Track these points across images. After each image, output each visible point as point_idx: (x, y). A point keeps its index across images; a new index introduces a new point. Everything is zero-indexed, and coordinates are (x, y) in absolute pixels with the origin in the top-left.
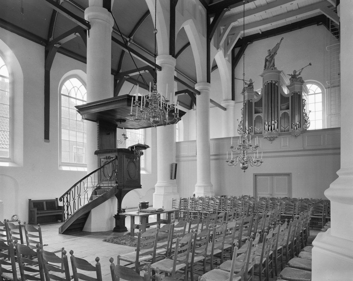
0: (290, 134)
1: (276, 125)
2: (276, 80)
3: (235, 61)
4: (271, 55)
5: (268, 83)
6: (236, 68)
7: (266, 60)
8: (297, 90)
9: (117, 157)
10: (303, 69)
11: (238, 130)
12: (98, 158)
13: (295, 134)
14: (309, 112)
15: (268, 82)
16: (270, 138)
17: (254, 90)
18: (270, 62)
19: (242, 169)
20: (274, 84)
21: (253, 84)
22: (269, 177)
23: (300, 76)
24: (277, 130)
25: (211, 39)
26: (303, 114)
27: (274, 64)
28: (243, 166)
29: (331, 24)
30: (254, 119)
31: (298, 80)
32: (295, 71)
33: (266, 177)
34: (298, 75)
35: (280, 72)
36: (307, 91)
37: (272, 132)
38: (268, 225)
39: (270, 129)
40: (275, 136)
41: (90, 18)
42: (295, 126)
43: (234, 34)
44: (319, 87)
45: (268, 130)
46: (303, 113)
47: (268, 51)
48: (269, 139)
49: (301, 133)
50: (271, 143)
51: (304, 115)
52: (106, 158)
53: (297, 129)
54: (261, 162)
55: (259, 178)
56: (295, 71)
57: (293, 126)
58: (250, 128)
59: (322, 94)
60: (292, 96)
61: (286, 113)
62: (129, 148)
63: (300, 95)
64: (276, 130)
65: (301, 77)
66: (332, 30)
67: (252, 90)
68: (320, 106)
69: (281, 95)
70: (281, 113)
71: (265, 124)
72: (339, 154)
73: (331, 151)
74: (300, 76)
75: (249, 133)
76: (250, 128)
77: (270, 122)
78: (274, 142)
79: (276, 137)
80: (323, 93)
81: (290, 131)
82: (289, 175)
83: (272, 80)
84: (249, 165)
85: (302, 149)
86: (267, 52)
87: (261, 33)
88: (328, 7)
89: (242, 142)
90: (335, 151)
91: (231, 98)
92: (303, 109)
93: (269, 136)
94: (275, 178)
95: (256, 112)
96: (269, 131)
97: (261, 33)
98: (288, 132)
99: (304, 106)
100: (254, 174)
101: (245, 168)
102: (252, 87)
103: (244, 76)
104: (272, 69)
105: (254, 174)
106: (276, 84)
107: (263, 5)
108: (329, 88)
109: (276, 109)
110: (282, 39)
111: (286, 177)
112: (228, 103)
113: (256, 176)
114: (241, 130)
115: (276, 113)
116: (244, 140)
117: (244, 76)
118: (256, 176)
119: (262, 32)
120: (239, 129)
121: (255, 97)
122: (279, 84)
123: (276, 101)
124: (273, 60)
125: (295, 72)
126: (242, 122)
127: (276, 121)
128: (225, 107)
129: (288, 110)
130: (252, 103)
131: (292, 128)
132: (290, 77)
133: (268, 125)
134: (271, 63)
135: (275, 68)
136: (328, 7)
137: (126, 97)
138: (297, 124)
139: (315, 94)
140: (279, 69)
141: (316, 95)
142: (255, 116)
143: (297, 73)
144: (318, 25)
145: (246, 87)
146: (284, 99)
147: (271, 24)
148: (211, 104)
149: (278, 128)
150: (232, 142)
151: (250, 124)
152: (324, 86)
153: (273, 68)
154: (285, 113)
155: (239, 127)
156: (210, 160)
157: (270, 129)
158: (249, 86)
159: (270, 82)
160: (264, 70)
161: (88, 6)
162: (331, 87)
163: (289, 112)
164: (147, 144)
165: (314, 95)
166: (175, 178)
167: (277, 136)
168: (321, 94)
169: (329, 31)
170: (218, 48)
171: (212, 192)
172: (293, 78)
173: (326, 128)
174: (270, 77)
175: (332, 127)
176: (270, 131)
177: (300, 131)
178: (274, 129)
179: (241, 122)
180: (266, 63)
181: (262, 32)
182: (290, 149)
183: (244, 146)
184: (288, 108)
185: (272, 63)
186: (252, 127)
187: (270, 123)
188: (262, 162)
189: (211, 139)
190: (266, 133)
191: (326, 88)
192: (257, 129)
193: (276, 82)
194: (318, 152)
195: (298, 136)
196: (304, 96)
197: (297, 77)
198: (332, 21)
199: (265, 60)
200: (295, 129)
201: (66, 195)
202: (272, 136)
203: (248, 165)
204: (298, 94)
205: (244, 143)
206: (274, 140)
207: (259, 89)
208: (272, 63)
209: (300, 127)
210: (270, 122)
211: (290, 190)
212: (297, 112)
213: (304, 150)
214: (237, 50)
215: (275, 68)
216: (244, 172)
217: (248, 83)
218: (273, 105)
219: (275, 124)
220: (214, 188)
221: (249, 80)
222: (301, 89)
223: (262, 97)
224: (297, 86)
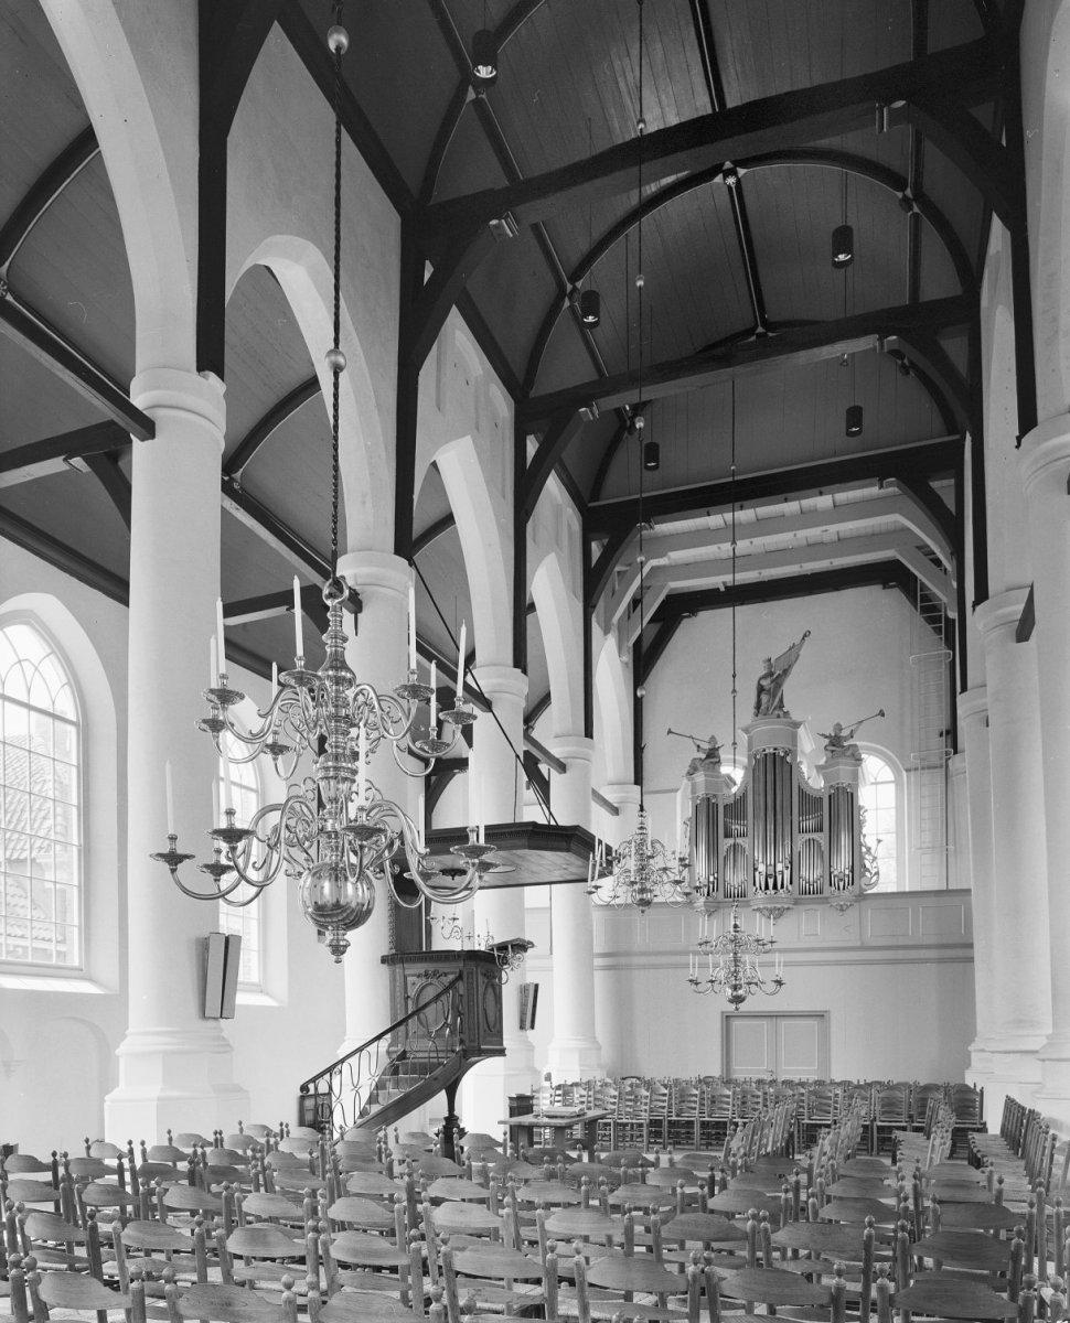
0: (826, 900)
1: (787, 874)
3: (643, 661)
5: (766, 755)
8: (845, 781)
9: (460, 977)
12: (393, 980)
22: (765, 1023)
23: (851, 742)
24: (790, 888)
27: (781, 700)
28: (735, 993)
31: (849, 753)
32: (838, 725)
34: (846, 739)
38: (595, 1216)
40: (786, 906)
41: (360, 581)
45: (767, 887)
46: (861, 845)
51: (864, 850)
52: (426, 975)
56: (838, 725)
58: (711, 879)
59: (897, 785)
62: (492, 950)
66: (924, 610)
69: (801, 792)
70: (800, 839)
71: (755, 869)
72: (971, 960)
73: (932, 954)
74: (851, 742)
75: (708, 895)
78: (782, 921)
79: (788, 909)
80: (898, 782)
81: (826, 894)
82: (820, 1016)
83: (775, 746)
85: (859, 944)
87: (722, 589)
88: (917, 547)
90: (960, 953)
93: (769, 906)
95: (727, 835)
96: (768, 892)
97: (722, 589)
100: (723, 1012)
104: (779, 716)
105: (723, 1012)
106: (788, 759)
107: (744, 523)
108: (916, 769)
109: (787, 828)
110: (805, 636)
111: (813, 1023)
115: (788, 841)
122: (795, 758)
125: (839, 727)
128: (615, 805)
129: (820, 834)
132: (827, 741)
134: (774, 697)
136: (917, 547)
137: (531, 828)
140: (795, 717)
143: (845, 733)
144: (884, 588)
146: (810, 802)
149: (791, 883)
153: (781, 713)
156: (592, 968)
158: (708, 757)
159: (772, 751)
161: (346, 553)
163: (822, 838)
164: (527, 938)
166: (532, 1027)
168: (892, 786)
169: (916, 609)
170: (606, 631)
171: (599, 1066)
174: (768, 735)
178: (782, 887)
180: (759, 696)
182: (825, 945)
185: (777, 700)
190: (761, 894)
193: (787, 754)
194: (900, 954)
195: (848, 907)
198: (922, 584)
201: (327, 1076)
202: (779, 906)
207: (735, 772)
208: (777, 700)
211: (825, 1062)
212: (844, 840)
213: (863, 948)
215: (786, 714)
217: (706, 746)
218: (779, 817)
219: (785, 871)
220: (607, 1054)
221: (707, 739)
222: (855, 776)
224: (843, 769)
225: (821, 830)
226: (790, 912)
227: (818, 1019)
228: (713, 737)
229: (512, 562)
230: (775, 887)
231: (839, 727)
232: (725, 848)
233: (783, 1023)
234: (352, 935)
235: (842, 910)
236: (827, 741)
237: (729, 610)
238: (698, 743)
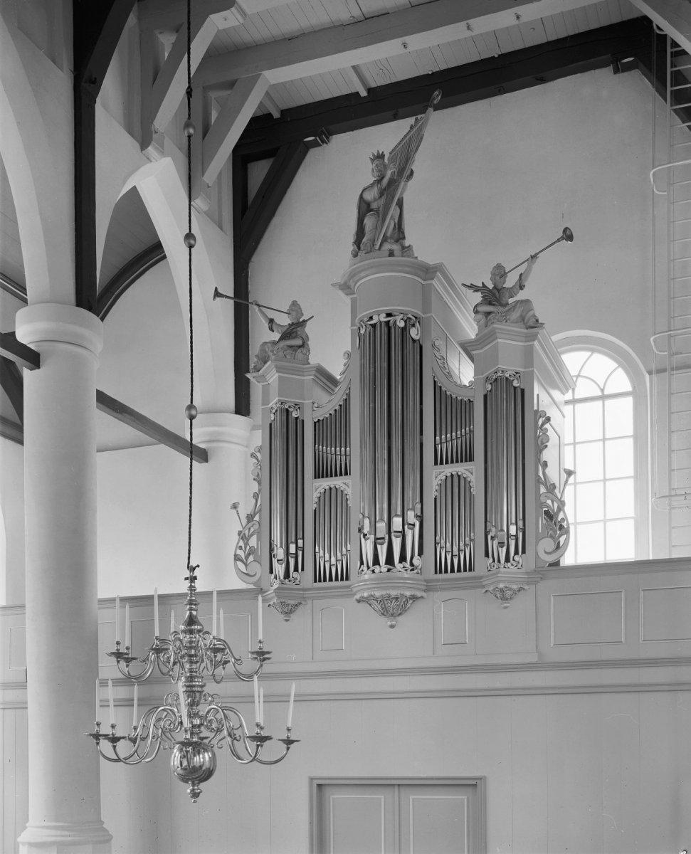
0: (477, 583)
2: (414, 310)
4: (385, 181)
5: (374, 326)
6: (254, 259)
7: (365, 208)
8: (508, 365)
10: (534, 257)
11: (237, 558)
13: (501, 586)
14: (564, 476)
15: (371, 318)
16: (381, 600)
17: (314, 360)
18: (382, 215)
19: (185, 779)
20: (404, 329)
21: (309, 329)
22: (381, 797)
23: (521, 296)
24: (416, 561)
25: (96, 83)
26: (538, 489)
27: (399, 227)
29: (673, 66)
30: (310, 505)
31: (515, 315)
32: (499, 267)
33: (368, 796)
34: (512, 293)
35: (428, 271)
36: (560, 380)
37: (394, 573)
39: (382, 559)
40: (408, 593)
42: (502, 545)
43: (231, 85)
44: (620, 365)
46: (538, 481)
47: (372, 160)
48: (378, 606)
49: (528, 583)
50: (392, 627)
51: (543, 490)
53: (507, 560)
54: (289, 742)
55: (335, 798)
56: (499, 267)
57: (494, 545)
58: (292, 549)
60: (485, 396)
61: (459, 476)
63: (523, 391)
64: (412, 564)
65: (527, 302)
67: (299, 354)
68: (623, 456)
70: (436, 476)
74: (521, 296)
75: (287, 575)
76: (292, 549)
77: (382, 519)
79: (414, 598)
80: (637, 394)
83: (389, 308)
84: (223, 755)
85: (533, 658)
86: (370, 166)
87: (363, 93)
89: (183, 627)
91: (229, 399)
92: (538, 459)
93: (378, 594)
94: (413, 797)
96: (377, 569)
97: (363, 93)
98: (468, 574)
99: (541, 446)
100: (312, 779)
101: (198, 776)
102: (298, 342)
103: (191, 247)
104: (391, 254)
105: (312, 779)
106: (414, 333)
108: (664, 370)
111: (462, 797)
112: (216, 429)
113: (321, 788)
114: (251, 558)
116: (191, 616)
117: (191, 247)
118: (321, 788)
119: (370, 90)
120: (241, 553)
121: (321, 396)
122: (426, 331)
123: (412, 416)
124: (394, 211)
125: (500, 272)
126: (257, 518)
127: (411, 516)
130: (299, 423)
131: (487, 555)
132: (478, 297)
133: (372, 537)
135: (403, 248)
138: (508, 536)
139: (603, 397)
141: (608, 402)
142: (315, 488)
143: (511, 281)
144: (616, 71)
145: (274, 343)
147: (405, 46)
148: (105, 426)
149: (421, 553)
150: (224, 618)
151: (293, 529)
152: (644, 363)
153: (396, 247)
154: (456, 479)
155: (241, 543)
157: (382, 559)
158: (285, 336)
159: (383, 318)
160: (355, 255)
162: (672, 369)
165: (599, 403)
167: (419, 594)
172: (490, 304)
173: (651, 558)
175: (675, 555)
176: (384, 568)
177: (523, 570)
178: (403, 559)
179: (250, 518)
181: (370, 90)
183: (191, 648)
184: (468, 457)
185: (389, 224)
186: (300, 542)
187: (382, 526)
188: (292, 742)
189: (101, 601)
190: (367, 575)
191: (650, 373)
192: (330, 560)
196: (542, 397)
197: (511, 301)
199: (359, 208)
200: (499, 561)
202: (394, 593)
203: (213, 759)
204: (516, 384)
205: (191, 632)
206: (403, 610)
208: (389, 224)
209: (524, 552)
210: (382, 519)
212: (506, 475)
214: (259, 172)
215: (406, 250)
216: (195, 795)
217: (284, 321)
219: (409, 534)
222: (529, 355)
223: (348, 395)
225: (471, 459)
226: (419, 604)
227: (470, 790)
228: (294, 304)
229: (232, 224)
230: (390, 560)
231: (500, 272)
232: (316, 495)
233: (411, 797)
234: (203, 786)
235: (504, 599)
236: (478, 297)
237: (616, 365)
238: (271, 314)
